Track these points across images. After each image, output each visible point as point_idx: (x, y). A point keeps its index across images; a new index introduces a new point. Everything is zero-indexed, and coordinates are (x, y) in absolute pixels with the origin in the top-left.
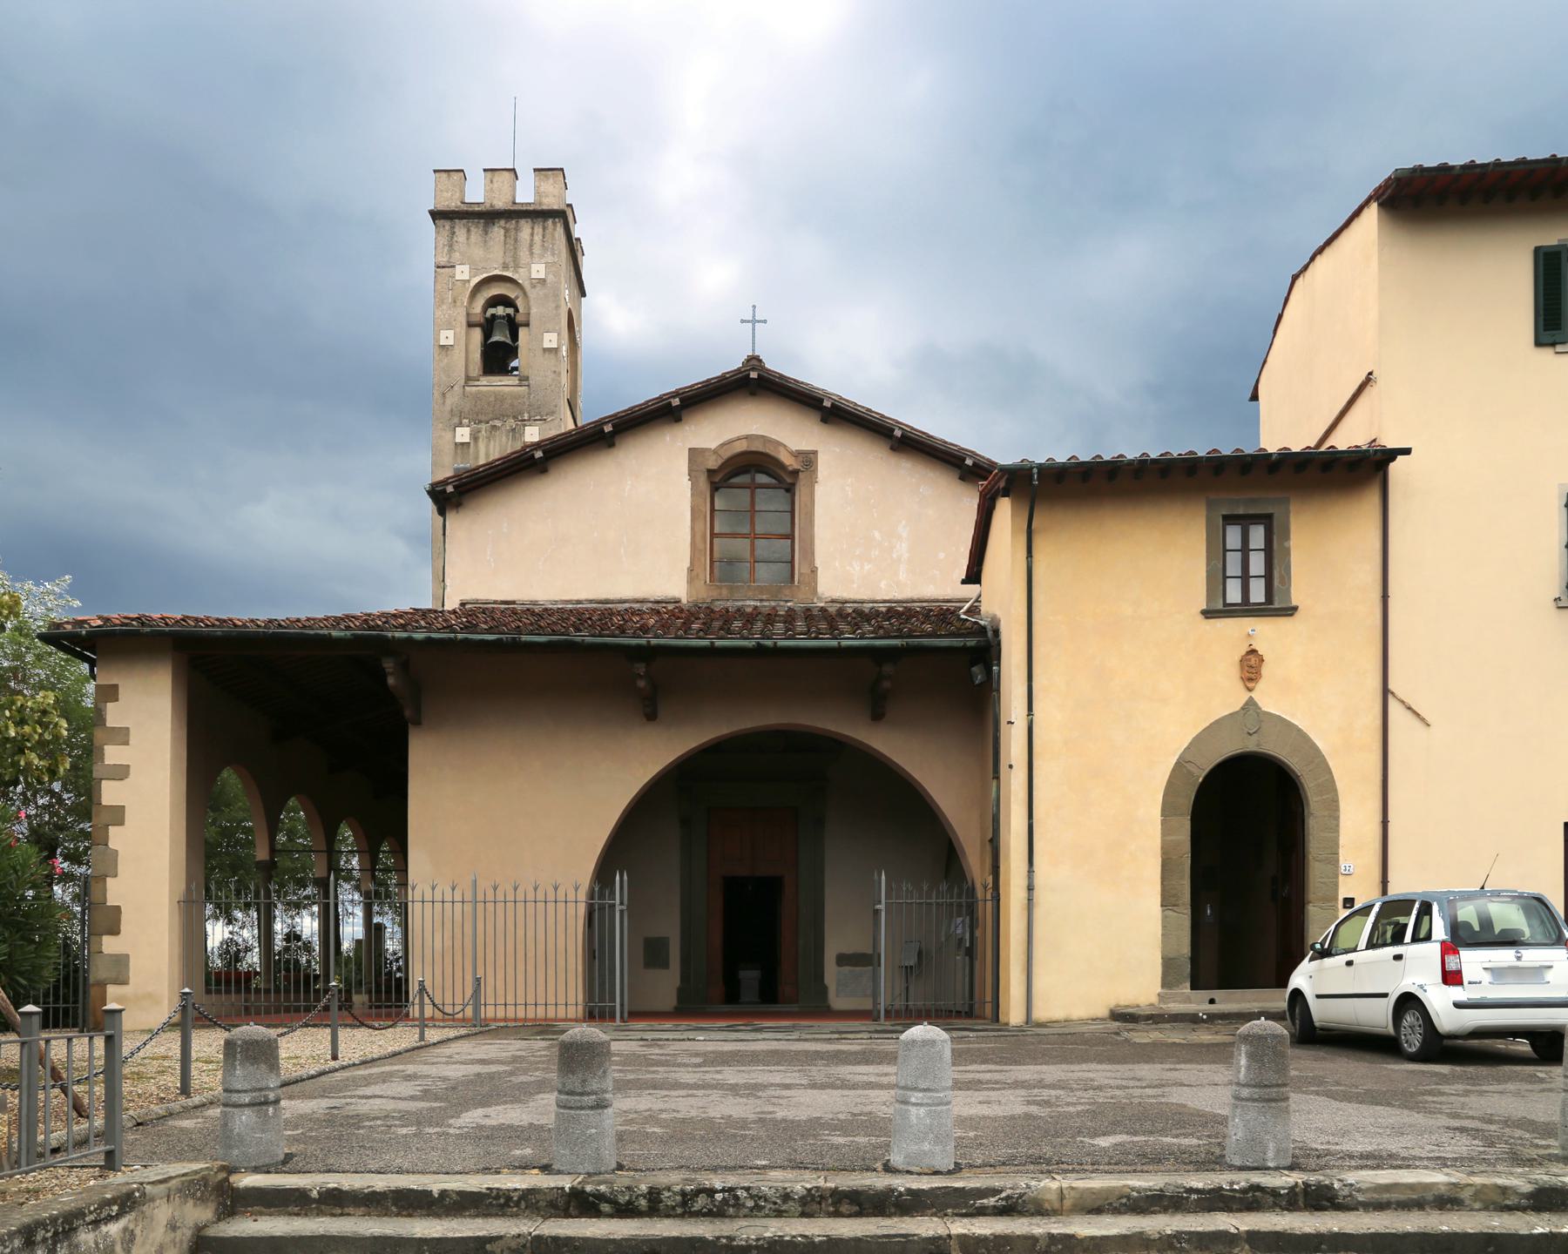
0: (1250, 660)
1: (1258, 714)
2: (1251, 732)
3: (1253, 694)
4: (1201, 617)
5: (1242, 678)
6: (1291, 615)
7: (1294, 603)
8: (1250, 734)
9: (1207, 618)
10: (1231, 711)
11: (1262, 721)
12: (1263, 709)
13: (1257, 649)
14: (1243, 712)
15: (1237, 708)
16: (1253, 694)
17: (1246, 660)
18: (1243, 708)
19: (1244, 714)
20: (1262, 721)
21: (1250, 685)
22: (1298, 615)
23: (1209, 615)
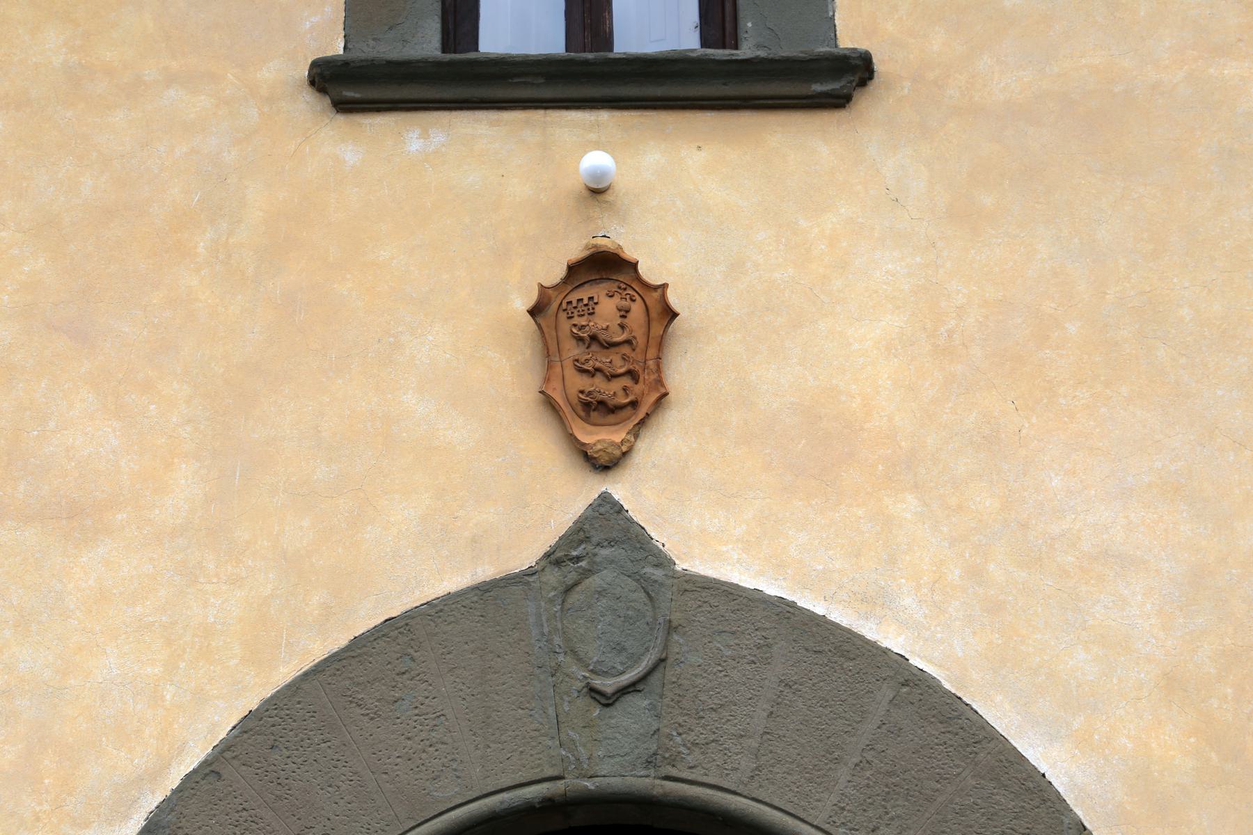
0: (590, 308)
1: (649, 589)
2: (608, 685)
3: (620, 488)
4: (309, 104)
5: (550, 403)
6: (839, 101)
7: (848, 38)
8: (607, 700)
9: (344, 106)
10: (486, 571)
11: (671, 628)
12: (680, 566)
13: (630, 253)
14: (553, 577)
15: (526, 556)
16: (620, 488)
17: (569, 309)
18: (553, 559)
19: (568, 590)
20: (671, 628)
21: (599, 437)
22: (867, 103)
23: (350, 94)
